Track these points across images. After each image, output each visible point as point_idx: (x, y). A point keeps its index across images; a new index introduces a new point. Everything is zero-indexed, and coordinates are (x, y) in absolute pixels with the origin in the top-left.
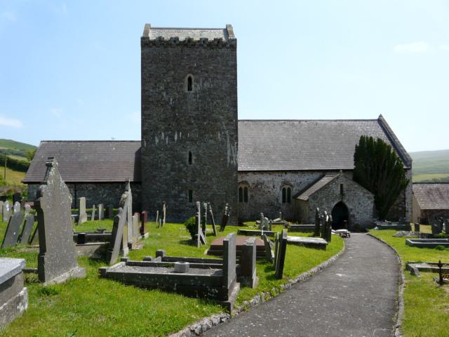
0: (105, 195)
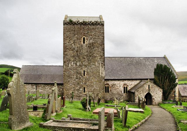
0: (48, 89)
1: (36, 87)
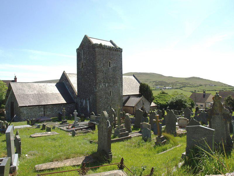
0: (57, 110)
1: (44, 109)
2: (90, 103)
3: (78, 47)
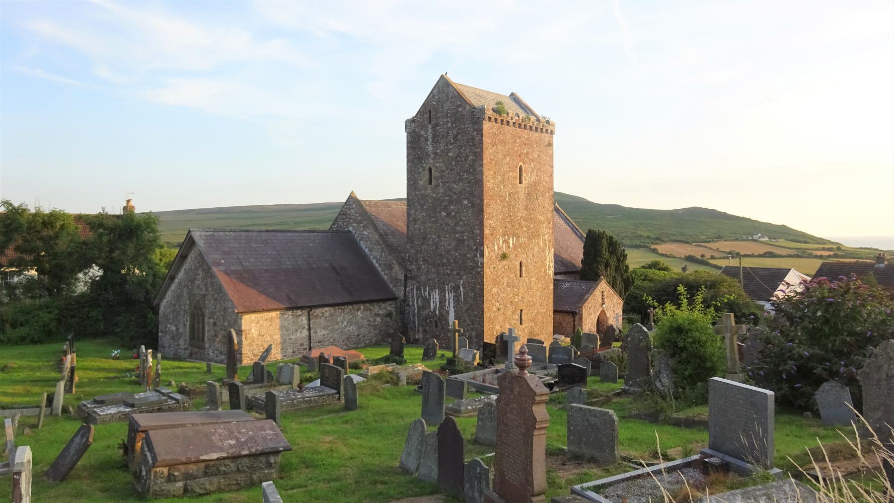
1: (309, 320)
2: (457, 299)
3: (412, 113)
